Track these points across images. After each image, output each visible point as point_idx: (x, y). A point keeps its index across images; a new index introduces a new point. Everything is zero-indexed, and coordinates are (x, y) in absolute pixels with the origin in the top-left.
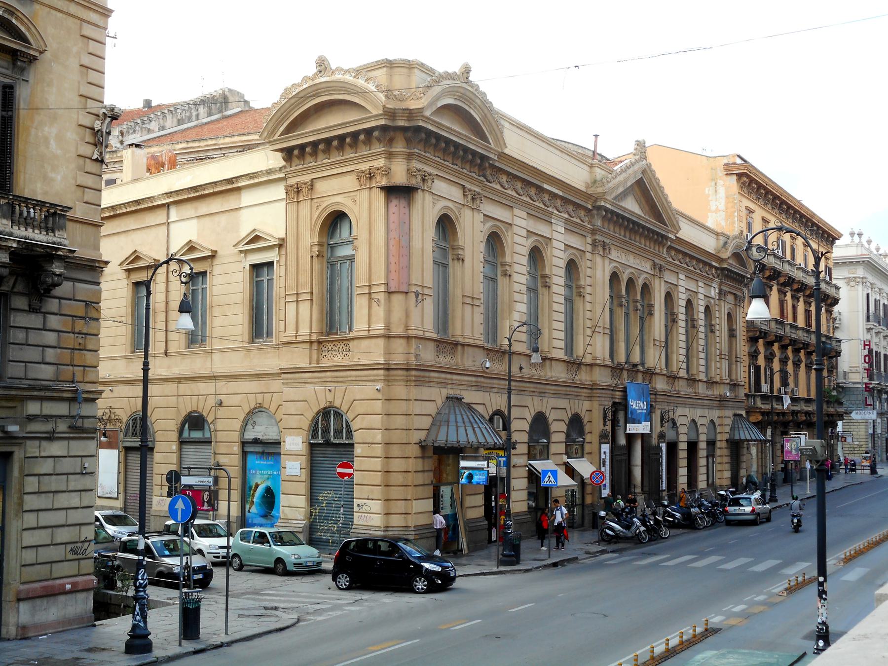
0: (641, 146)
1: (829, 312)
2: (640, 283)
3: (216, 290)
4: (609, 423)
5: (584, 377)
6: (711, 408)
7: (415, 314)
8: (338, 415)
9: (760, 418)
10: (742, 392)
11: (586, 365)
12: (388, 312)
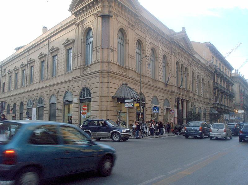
0: (184, 29)
1: (232, 87)
2: (185, 66)
3: (59, 59)
4: (177, 103)
5: (169, 88)
6: (204, 105)
7: (111, 55)
8: (87, 90)
9: (217, 109)
10: (212, 102)
11: (170, 85)
12: (102, 54)
